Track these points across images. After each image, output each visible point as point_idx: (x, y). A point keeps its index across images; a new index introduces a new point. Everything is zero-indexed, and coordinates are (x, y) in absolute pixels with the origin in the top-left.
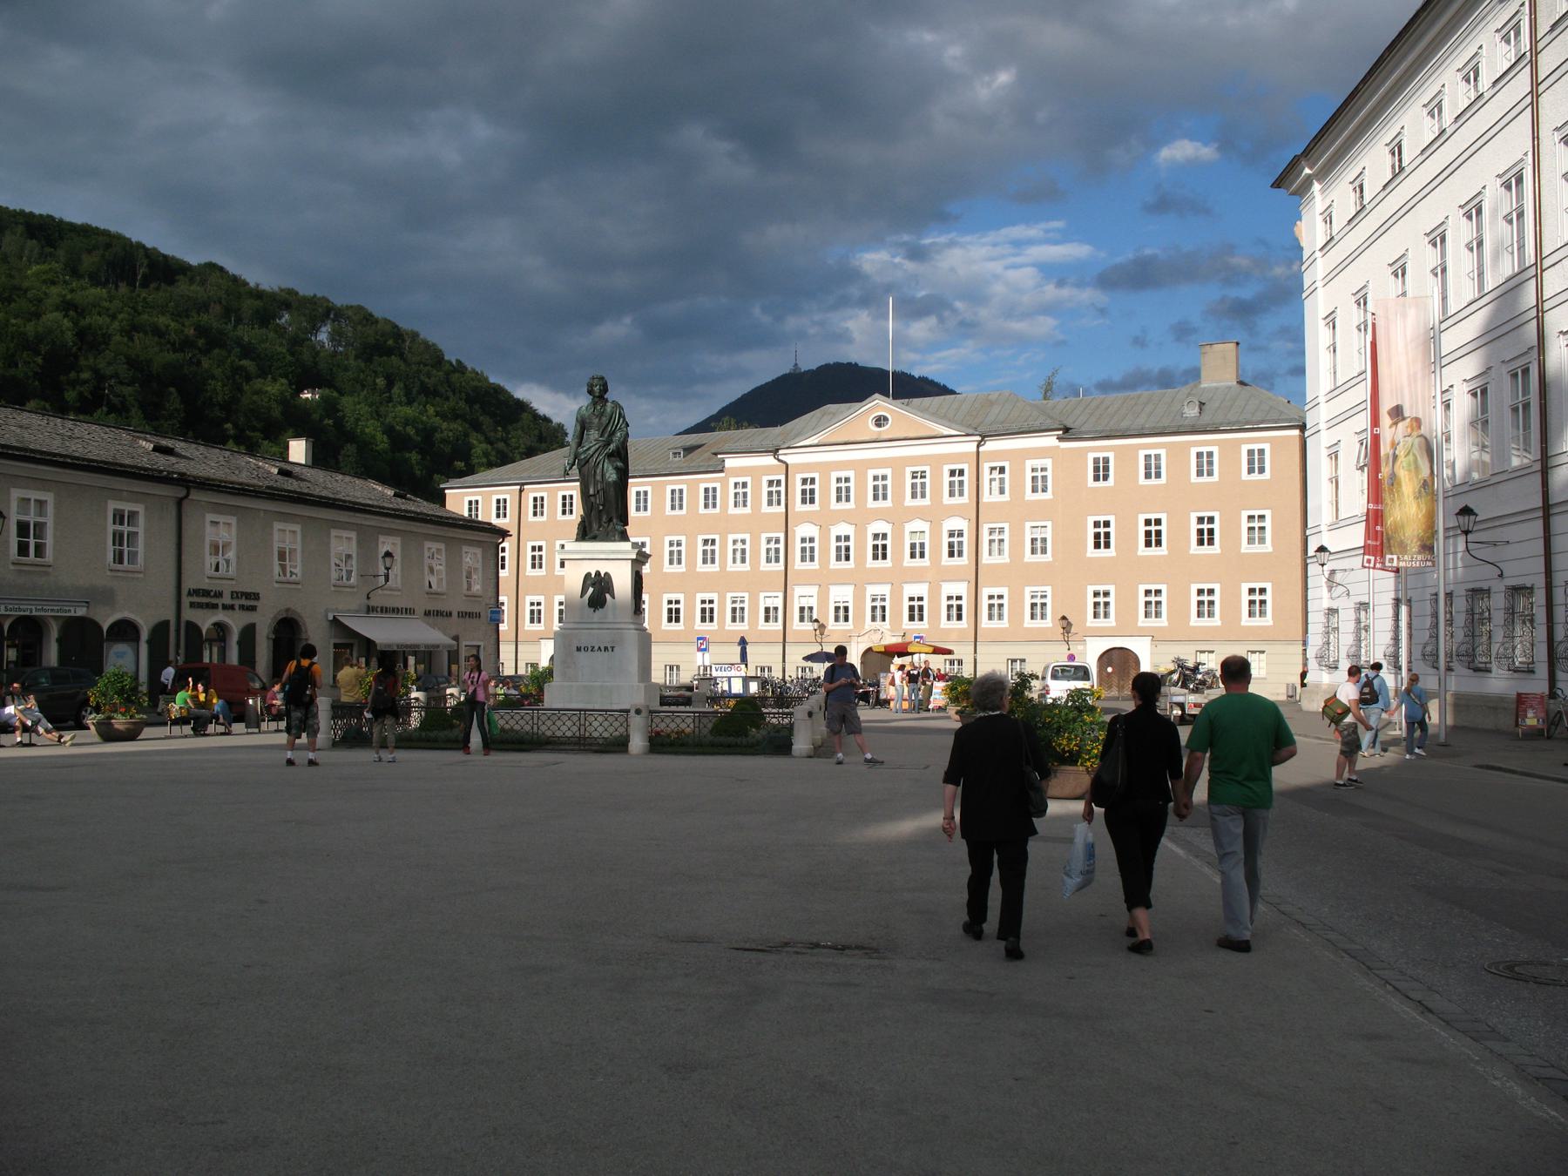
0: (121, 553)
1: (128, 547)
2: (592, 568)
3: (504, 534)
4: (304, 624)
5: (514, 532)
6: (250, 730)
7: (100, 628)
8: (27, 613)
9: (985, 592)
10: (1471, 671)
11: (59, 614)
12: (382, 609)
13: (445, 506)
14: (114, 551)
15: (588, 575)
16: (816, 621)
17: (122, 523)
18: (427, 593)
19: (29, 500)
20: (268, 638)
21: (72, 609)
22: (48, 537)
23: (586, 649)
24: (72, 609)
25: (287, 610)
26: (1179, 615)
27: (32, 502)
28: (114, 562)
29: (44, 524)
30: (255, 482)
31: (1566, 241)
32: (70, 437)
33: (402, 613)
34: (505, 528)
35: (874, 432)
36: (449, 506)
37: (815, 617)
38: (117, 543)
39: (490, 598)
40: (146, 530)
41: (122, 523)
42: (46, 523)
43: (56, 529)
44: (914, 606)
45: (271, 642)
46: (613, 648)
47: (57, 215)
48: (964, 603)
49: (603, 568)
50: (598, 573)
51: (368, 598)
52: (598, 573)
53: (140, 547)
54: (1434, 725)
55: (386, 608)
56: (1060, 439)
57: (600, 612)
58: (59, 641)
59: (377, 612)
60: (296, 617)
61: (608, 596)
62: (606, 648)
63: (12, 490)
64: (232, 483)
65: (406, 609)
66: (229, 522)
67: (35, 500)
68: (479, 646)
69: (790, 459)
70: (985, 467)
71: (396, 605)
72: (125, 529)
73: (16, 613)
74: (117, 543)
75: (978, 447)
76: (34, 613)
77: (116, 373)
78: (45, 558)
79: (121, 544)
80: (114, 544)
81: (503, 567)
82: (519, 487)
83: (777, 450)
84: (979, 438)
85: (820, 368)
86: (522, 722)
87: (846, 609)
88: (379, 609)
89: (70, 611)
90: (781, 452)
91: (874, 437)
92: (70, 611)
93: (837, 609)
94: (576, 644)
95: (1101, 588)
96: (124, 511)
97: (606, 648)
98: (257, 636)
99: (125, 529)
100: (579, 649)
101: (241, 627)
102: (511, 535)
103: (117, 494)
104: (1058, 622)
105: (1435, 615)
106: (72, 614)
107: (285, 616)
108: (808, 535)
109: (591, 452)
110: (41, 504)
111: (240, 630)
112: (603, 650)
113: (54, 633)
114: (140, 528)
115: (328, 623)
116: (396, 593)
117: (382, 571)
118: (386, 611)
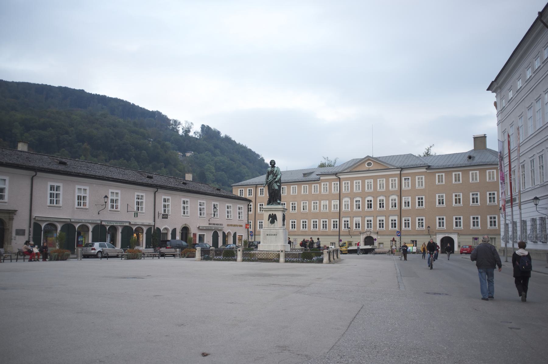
0: (138, 208)
1: (115, 203)
2: (271, 213)
3: (250, 201)
4: (190, 229)
5: (253, 200)
6: (76, 253)
7: (133, 229)
8: (113, 224)
9: (403, 219)
10: (541, 243)
11: (121, 225)
12: (213, 224)
13: (232, 193)
14: (111, 205)
15: (270, 214)
16: (349, 228)
17: (184, 204)
18: (227, 219)
19: (81, 189)
20: (180, 233)
21: (125, 223)
22: (61, 198)
23: (269, 235)
24: (125, 223)
25: (185, 224)
26: (467, 225)
27: (82, 189)
28: (111, 208)
29: (86, 197)
30: (176, 186)
31: (547, 70)
32: (124, 174)
33: (219, 225)
34: (250, 199)
35: (367, 167)
36: (233, 193)
37: (349, 227)
38: (112, 202)
39: (246, 221)
40: (206, 207)
41: (165, 202)
42: (86, 196)
43: (121, 201)
44: (381, 223)
45: (181, 234)
46: (277, 234)
47: (164, 113)
48: (397, 222)
49: (274, 213)
50: (273, 214)
51: (209, 221)
52: (273, 214)
53: (144, 206)
54: (456, 251)
55: (220, 224)
56: (426, 169)
57: (273, 225)
58: (122, 233)
59: (219, 225)
60: (187, 226)
61: (275, 221)
62: (275, 235)
63: (163, 196)
64: (170, 187)
65: (220, 224)
66: (5, 178)
67: (83, 189)
68: (242, 236)
69: (341, 177)
70: (403, 178)
71: (217, 223)
72: (140, 201)
73: (110, 224)
74: (112, 202)
75: (400, 172)
76: (115, 224)
77: (545, 218)
78: (4, 199)
79: (139, 205)
80: (111, 203)
81: (251, 211)
82: (255, 186)
83: (337, 174)
84: (400, 169)
85: (60, 88)
86: (262, 256)
87: (359, 224)
88: (212, 224)
89: (124, 224)
90: (338, 174)
91: (367, 169)
92: (124, 224)
93: (356, 224)
94: (266, 233)
95: (420, 218)
96: (54, 186)
97: (275, 235)
98: (177, 232)
99: (140, 201)
100: (267, 235)
101: (172, 229)
102: (252, 202)
103: (184, 196)
104: (426, 228)
105: (40, 155)
106: (125, 225)
107: (184, 226)
108: (369, 199)
109: (271, 181)
110: (85, 190)
111: (172, 230)
112: (274, 235)
113: (120, 230)
114: (61, 192)
115: (197, 228)
116: (217, 219)
117: (213, 213)
118: (214, 225)
